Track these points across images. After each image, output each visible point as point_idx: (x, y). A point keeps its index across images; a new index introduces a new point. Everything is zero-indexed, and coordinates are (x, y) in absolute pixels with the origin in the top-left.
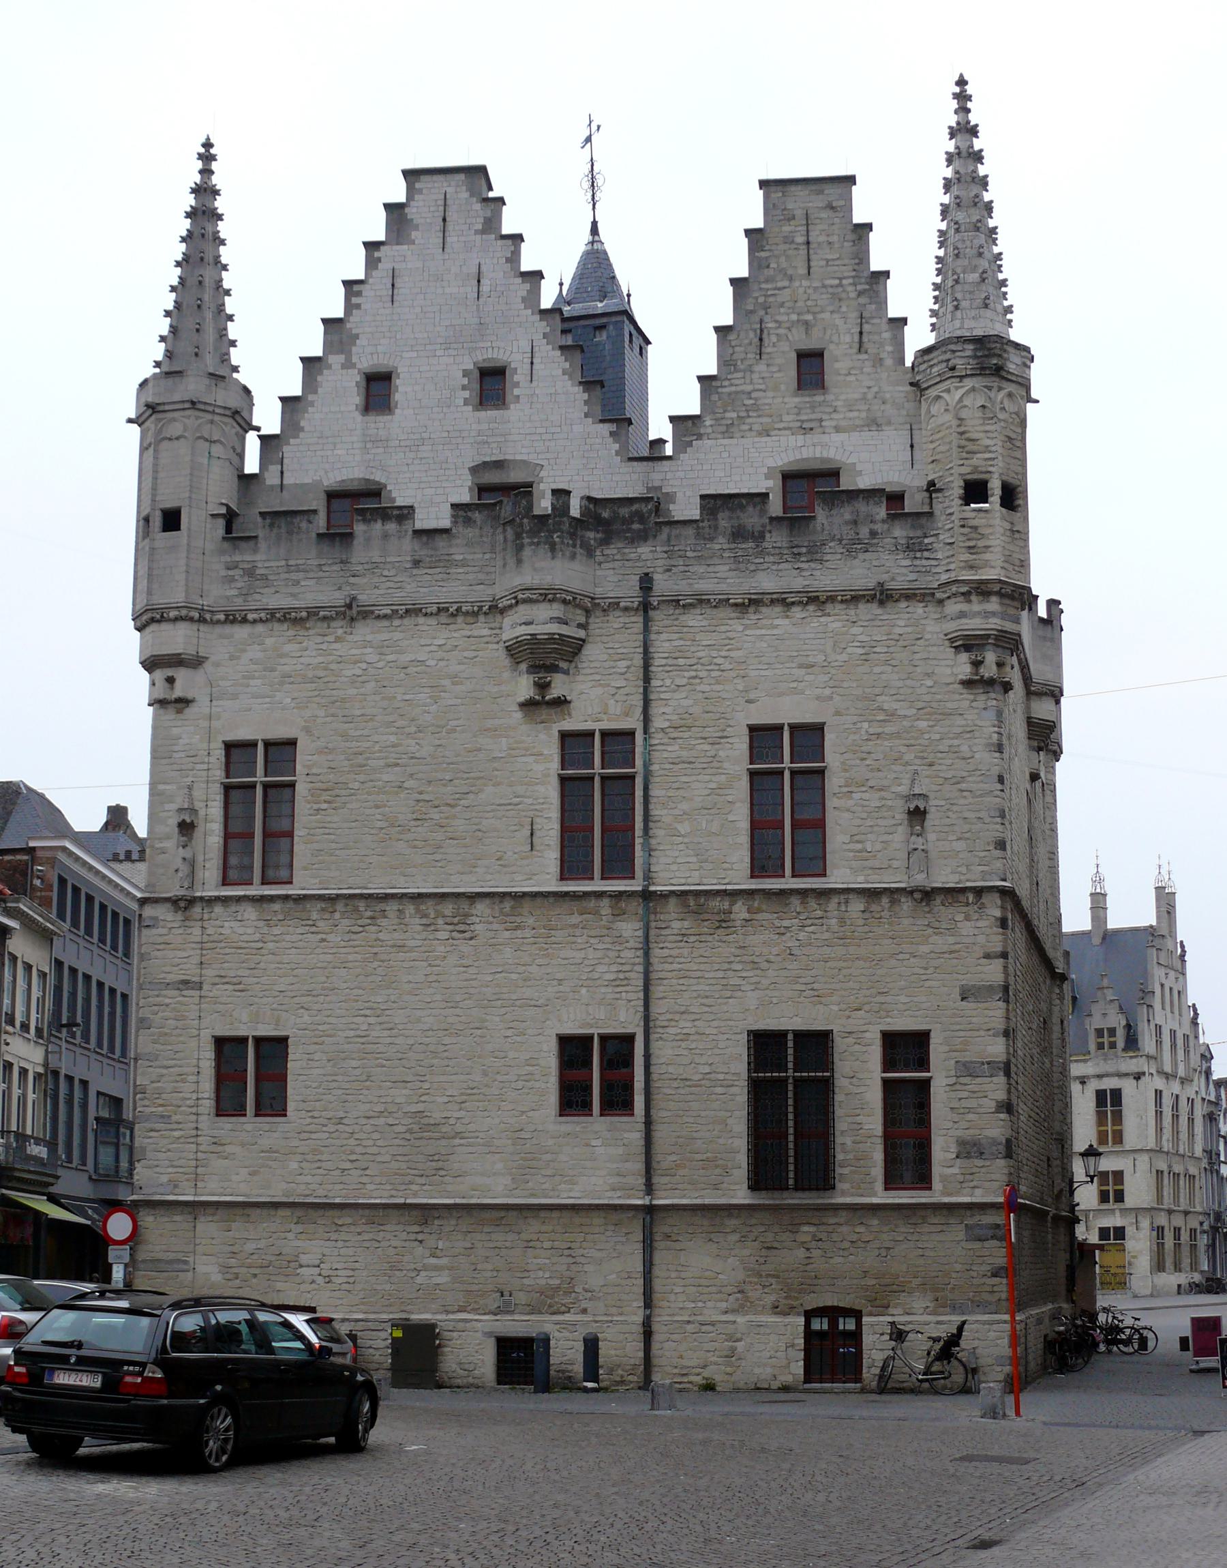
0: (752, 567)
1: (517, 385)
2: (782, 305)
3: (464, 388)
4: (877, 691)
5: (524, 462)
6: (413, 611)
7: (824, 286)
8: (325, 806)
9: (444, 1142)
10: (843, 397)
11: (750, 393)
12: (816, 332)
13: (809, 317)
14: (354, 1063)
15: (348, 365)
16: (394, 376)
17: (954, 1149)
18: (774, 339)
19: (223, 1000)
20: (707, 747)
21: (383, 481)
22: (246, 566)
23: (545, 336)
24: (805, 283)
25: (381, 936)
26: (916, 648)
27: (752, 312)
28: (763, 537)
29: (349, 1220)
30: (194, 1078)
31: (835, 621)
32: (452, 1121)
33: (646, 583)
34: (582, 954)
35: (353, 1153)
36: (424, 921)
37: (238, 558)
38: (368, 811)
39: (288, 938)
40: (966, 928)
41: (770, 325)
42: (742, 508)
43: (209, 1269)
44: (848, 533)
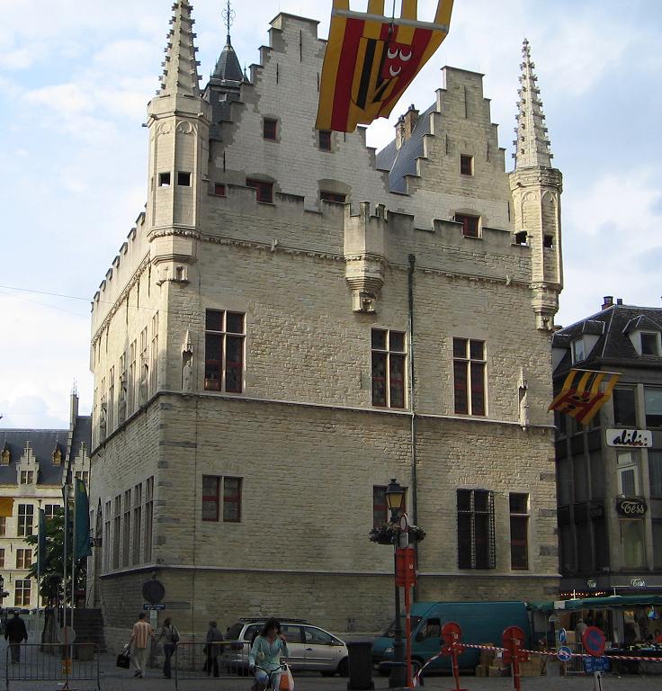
0: (456, 259)
5: (342, 183)
6: (304, 254)
9: (322, 540)
12: (470, 147)
13: (465, 139)
14: (277, 495)
15: (256, 111)
16: (278, 122)
17: (539, 550)
21: (275, 178)
25: (290, 426)
27: (442, 130)
29: (274, 581)
32: (325, 528)
34: (384, 445)
35: (277, 544)
40: (541, 446)
43: (201, 608)
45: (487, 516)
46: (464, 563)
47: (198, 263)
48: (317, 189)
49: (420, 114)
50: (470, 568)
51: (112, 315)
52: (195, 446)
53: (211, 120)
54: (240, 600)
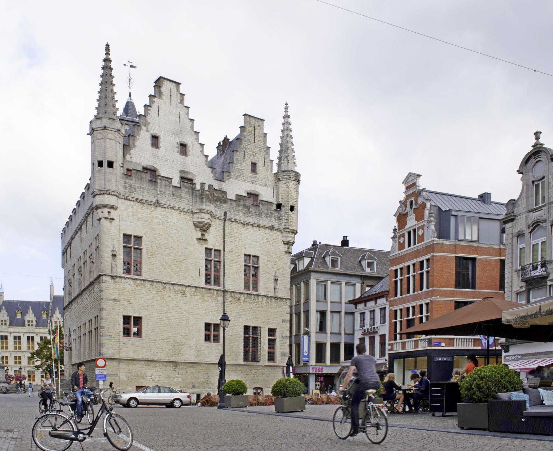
3: (177, 147)
4: (270, 251)
7: (258, 147)
9: (180, 347)
11: (241, 170)
13: (254, 154)
14: (159, 325)
15: (147, 131)
17: (280, 354)
18: (247, 157)
20: (236, 257)
21: (157, 168)
22: (130, 184)
33: (225, 214)
34: (210, 304)
35: (159, 348)
37: (127, 181)
38: (161, 260)
39: (142, 291)
40: (284, 307)
45: (257, 338)
46: (246, 359)
47: (118, 209)
49: (230, 141)
50: (249, 361)
51: (72, 239)
52: (119, 301)
53: (124, 133)
54: (141, 373)
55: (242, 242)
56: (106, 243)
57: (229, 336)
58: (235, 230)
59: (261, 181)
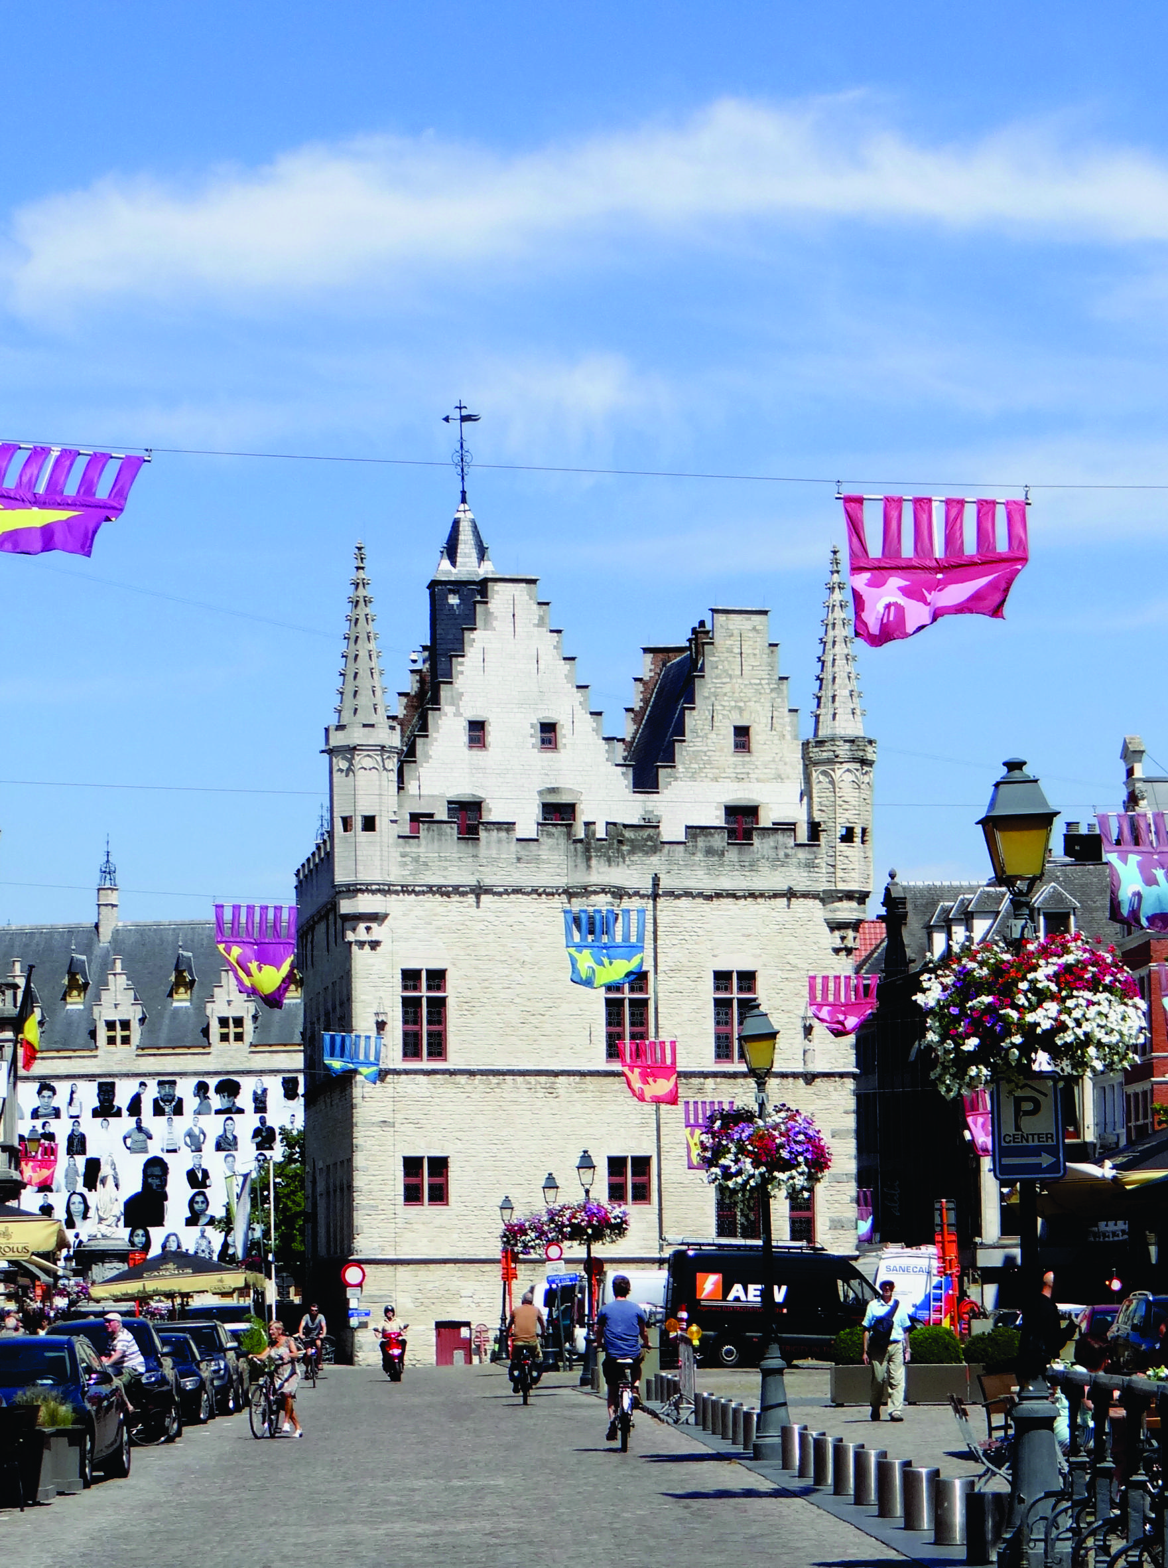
0: (717, 873)
1: (564, 736)
2: (725, 694)
3: (532, 736)
4: (786, 952)
7: (751, 684)
8: (466, 1013)
10: (761, 759)
11: (705, 752)
12: (746, 714)
13: (742, 704)
14: (489, 1173)
15: (458, 714)
17: (828, 1224)
18: (720, 717)
19: (409, 1133)
20: (691, 983)
22: (413, 855)
23: (581, 703)
24: (740, 681)
26: (808, 927)
28: (723, 854)
30: (392, 1183)
31: (762, 906)
33: (656, 880)
34: (620, 1108)
36: (529, 1086)
37: (408, 850)
38: (494, 1017)
39: (446, 1095)
40: (835, 1096)
41: (718, 708)
42: (712, 835)
44: (772, 854)
48: (538, 802)
55: (708, 942)
56: (363, 997)
57: (676, 1185)
58: (685, 914)
59: (766, 771)
